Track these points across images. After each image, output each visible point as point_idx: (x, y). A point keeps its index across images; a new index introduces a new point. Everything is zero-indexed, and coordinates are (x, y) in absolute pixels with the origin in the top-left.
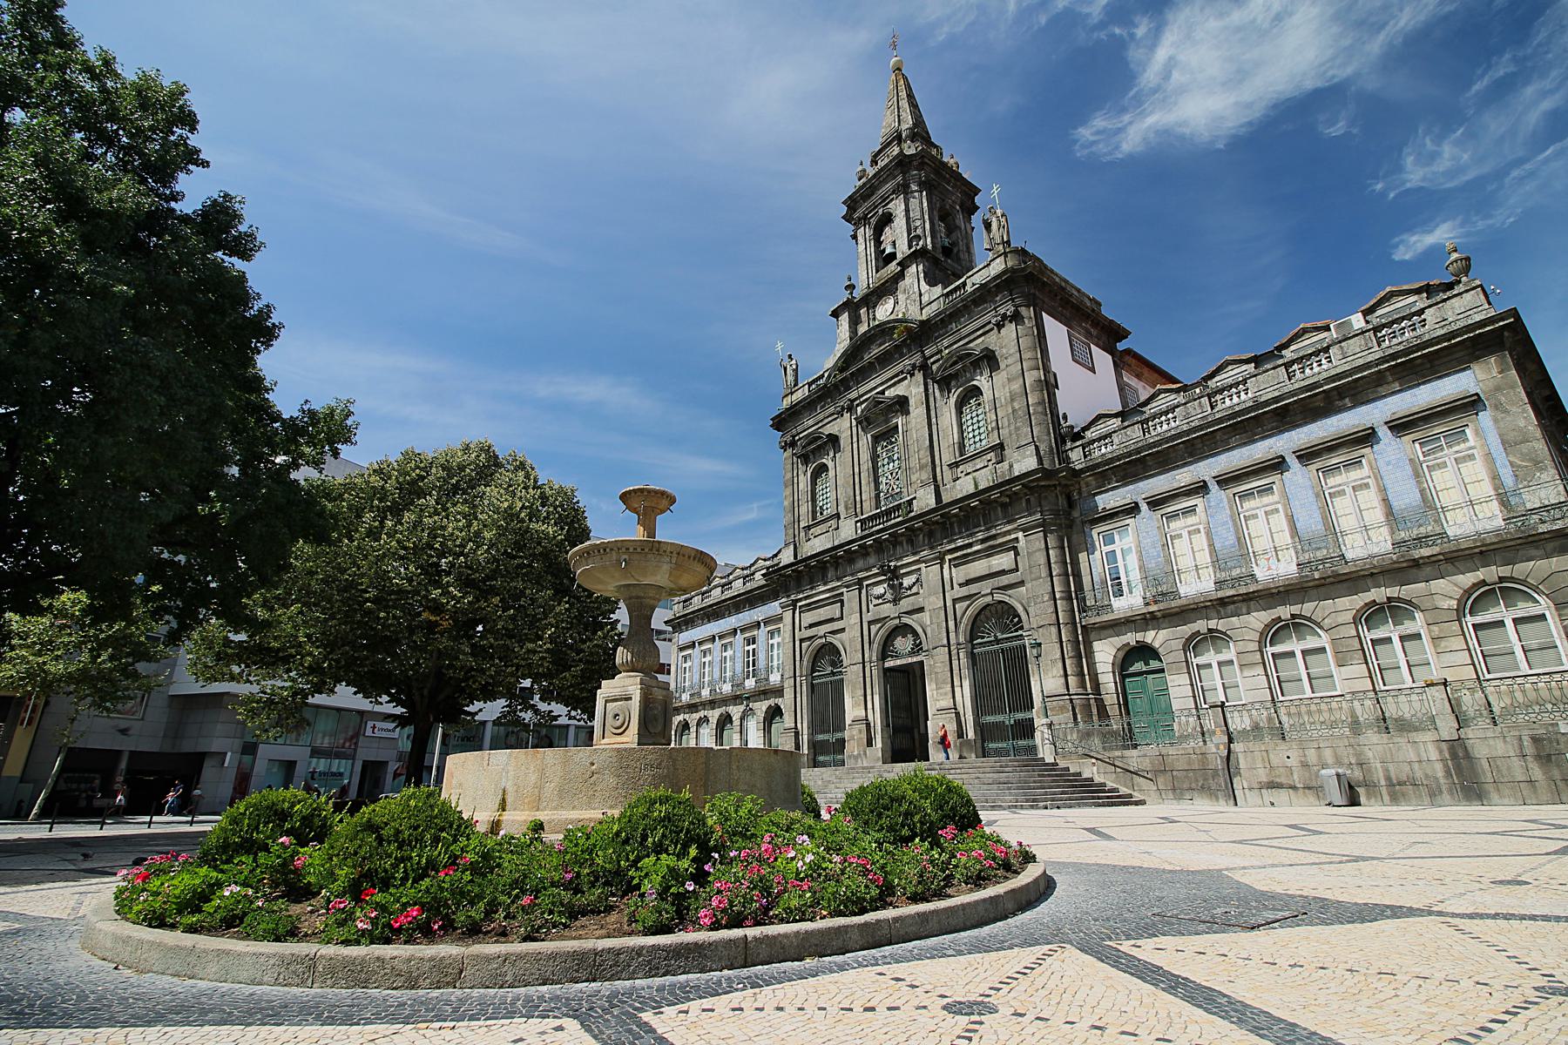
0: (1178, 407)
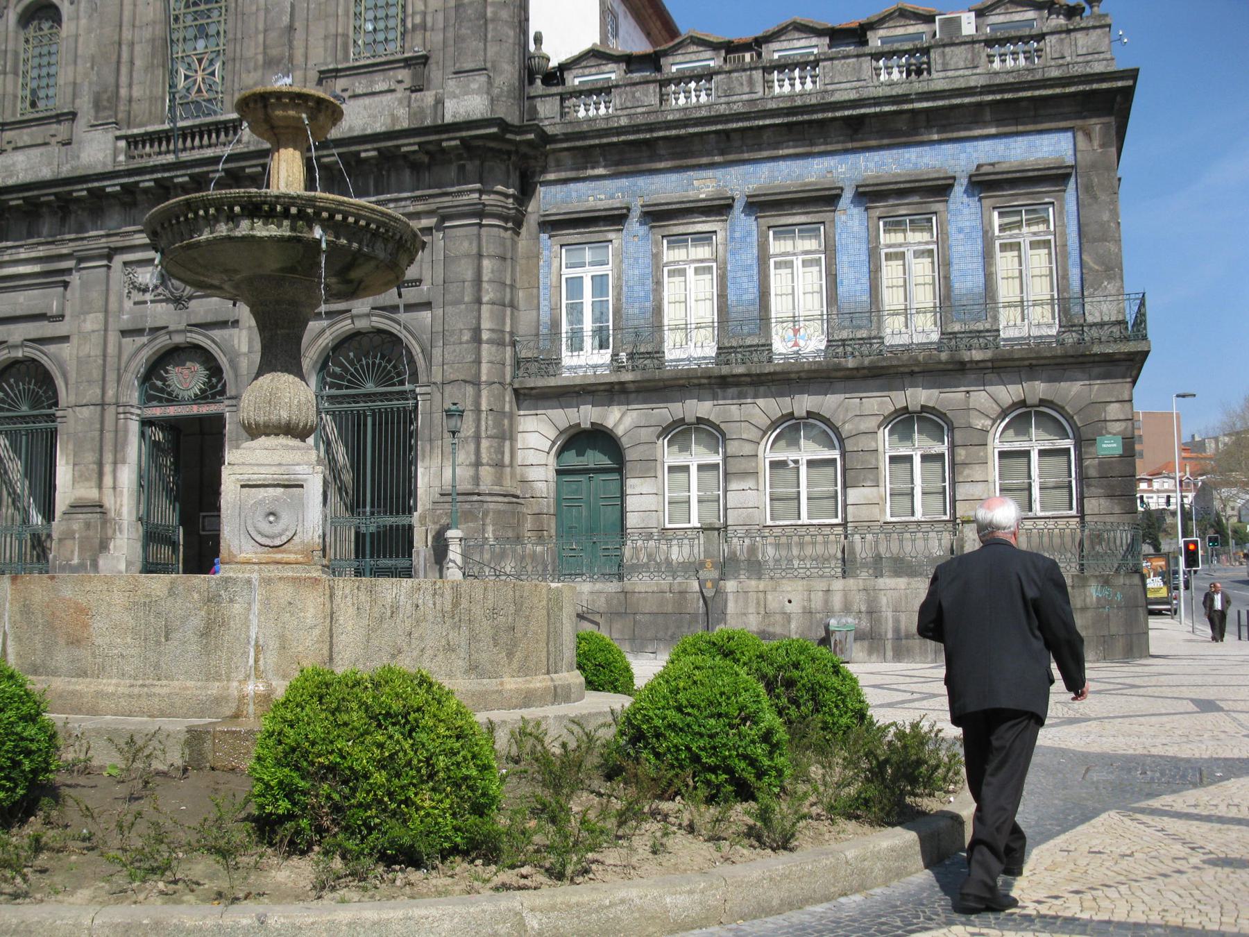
0: (717, 73)
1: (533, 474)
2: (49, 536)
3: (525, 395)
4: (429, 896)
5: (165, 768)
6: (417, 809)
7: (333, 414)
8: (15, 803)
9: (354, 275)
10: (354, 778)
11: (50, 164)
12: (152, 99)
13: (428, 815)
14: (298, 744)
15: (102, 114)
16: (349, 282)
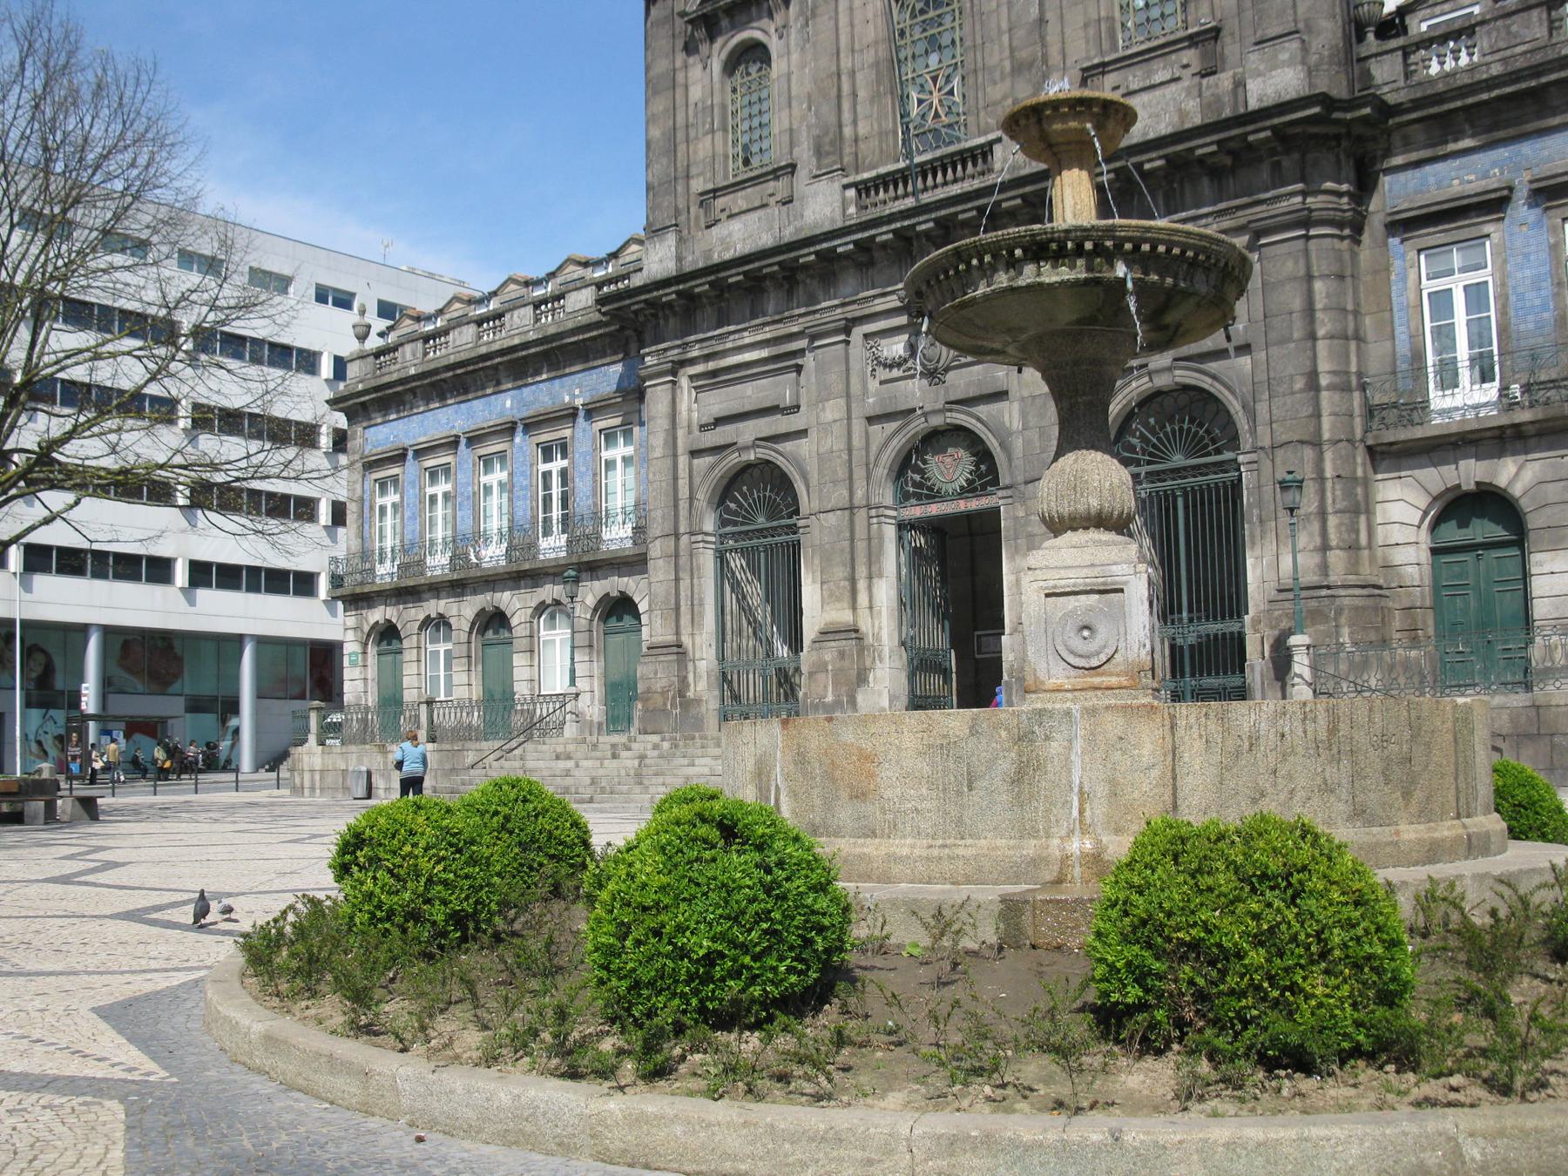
1: (1400, 556)
2: (797, 670)
3: (1382, 453)
4: (1327, 1111)
5: (976, 947)
6: (1307, 997)
7: (743, 552)
8: (807, 989)
9: (1170, 318)
10: (1224, 958)
11: (771, 228)
12: (882, 134)
13: (1320, 1005)
14: (1150, 916)
15: (826, 161)
16: (1166, 327)
